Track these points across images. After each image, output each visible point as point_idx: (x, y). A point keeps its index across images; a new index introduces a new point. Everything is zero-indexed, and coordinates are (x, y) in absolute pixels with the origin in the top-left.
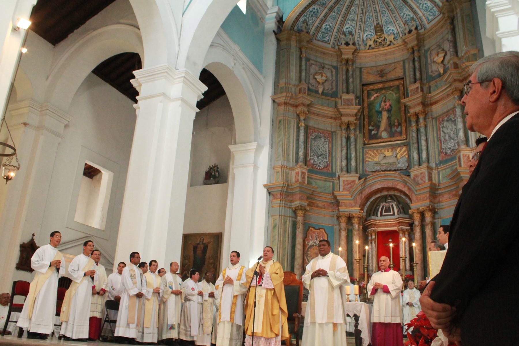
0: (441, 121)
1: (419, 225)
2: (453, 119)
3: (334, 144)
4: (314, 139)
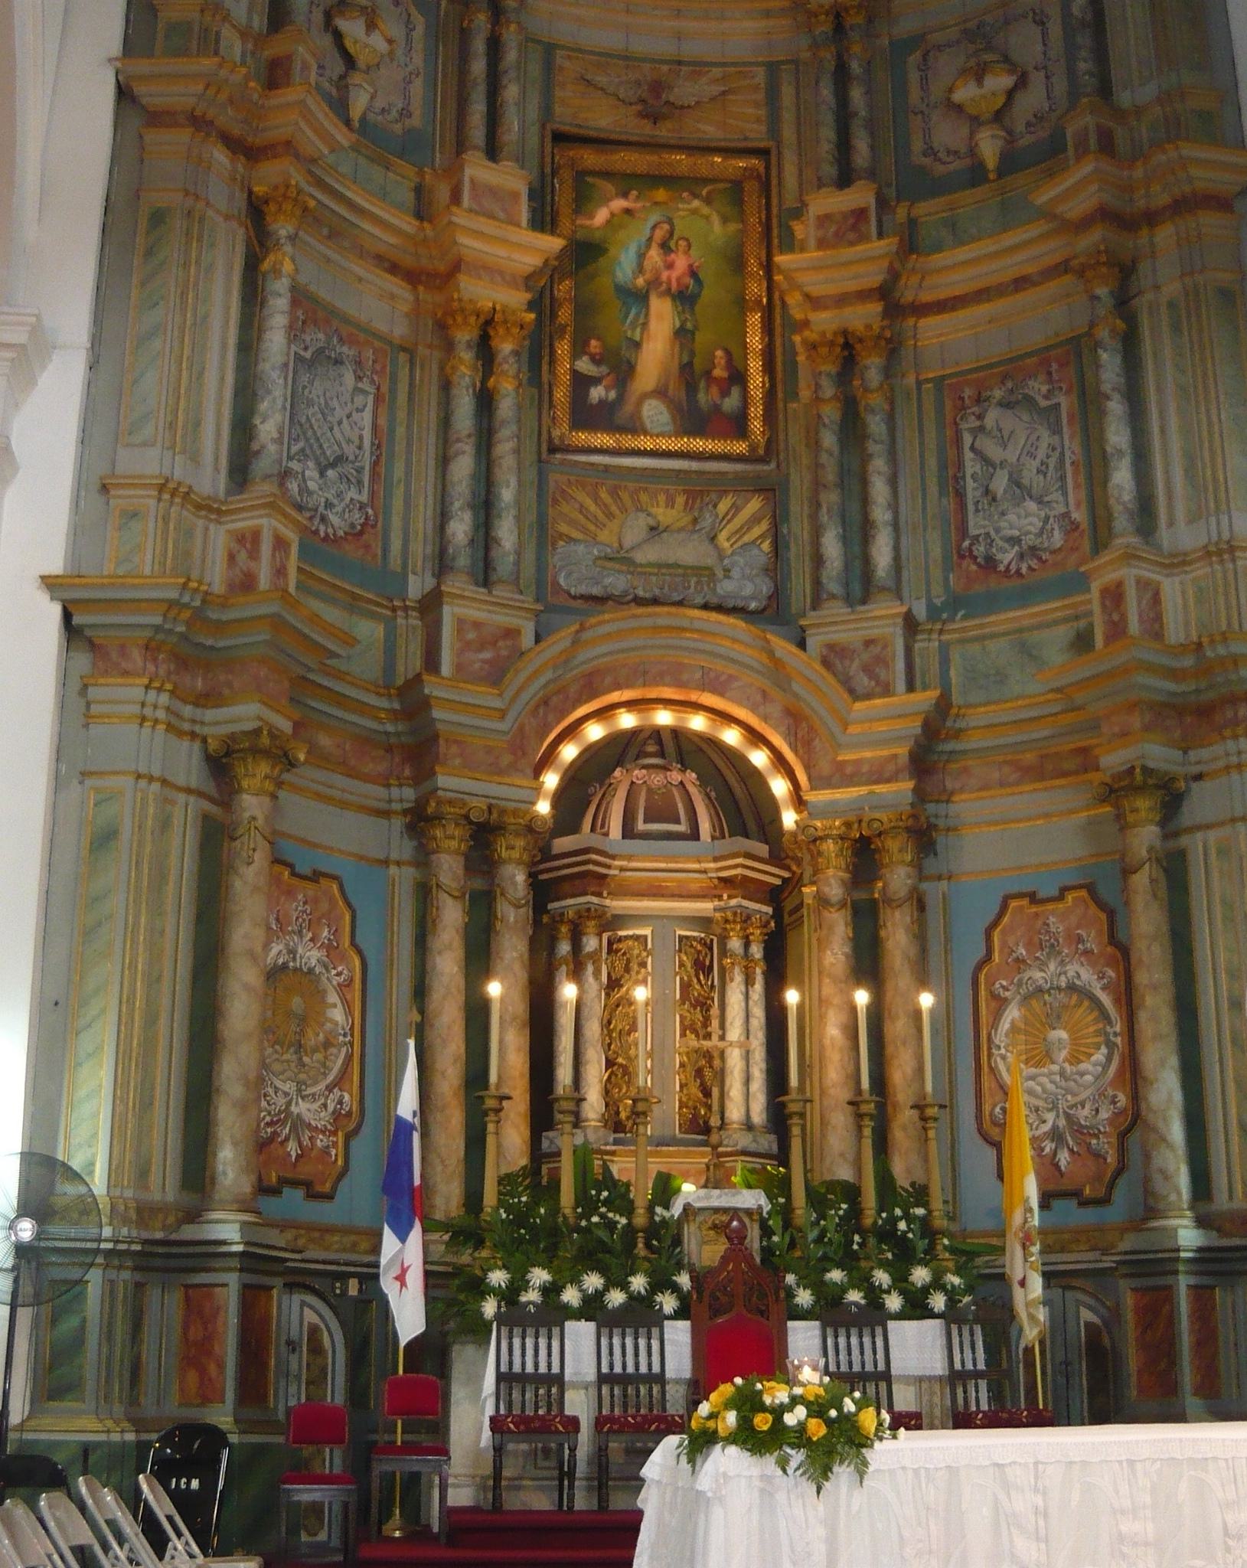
0: (967, 401)
2: (1043, 403)
3: (401, 415)
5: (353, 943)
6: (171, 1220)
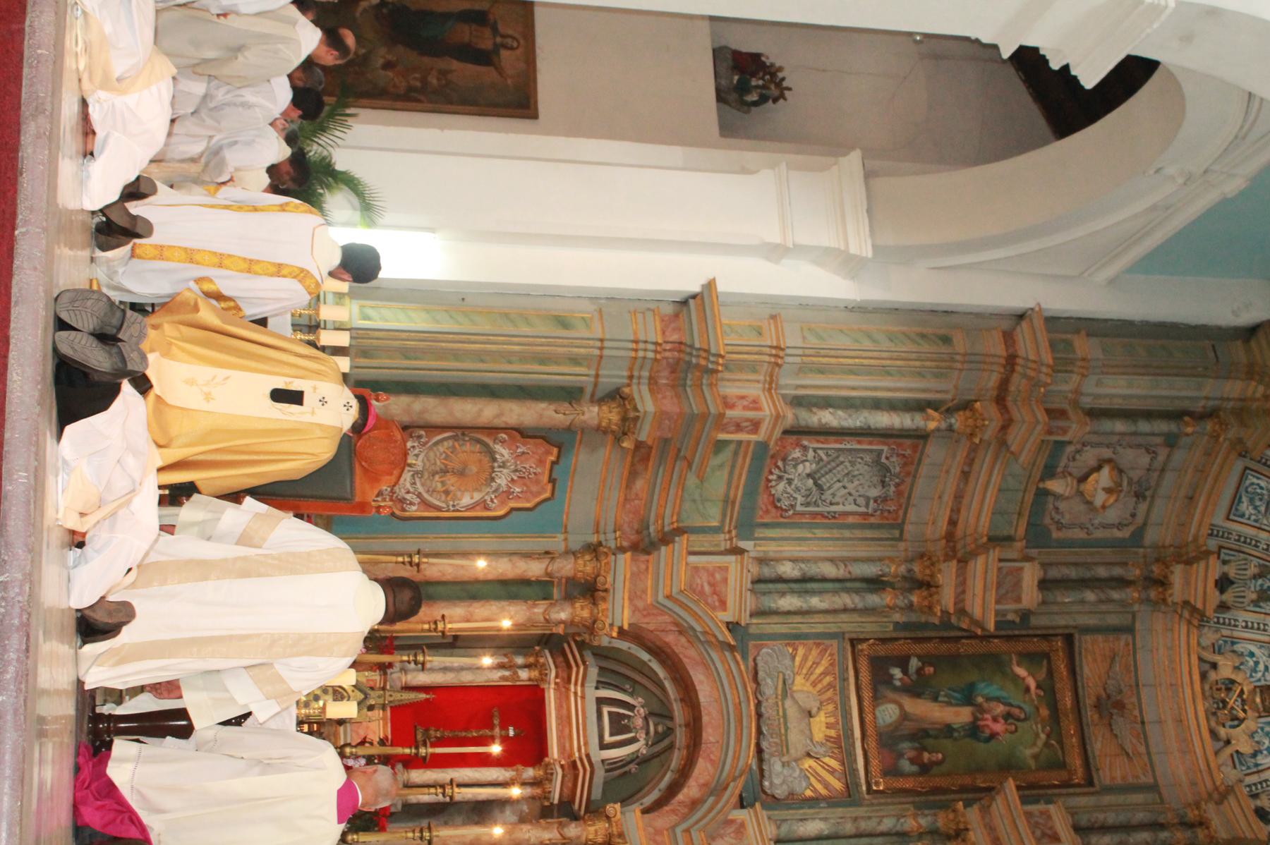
3: (858, 533)
4: (877, 462)
5: (513, 509)
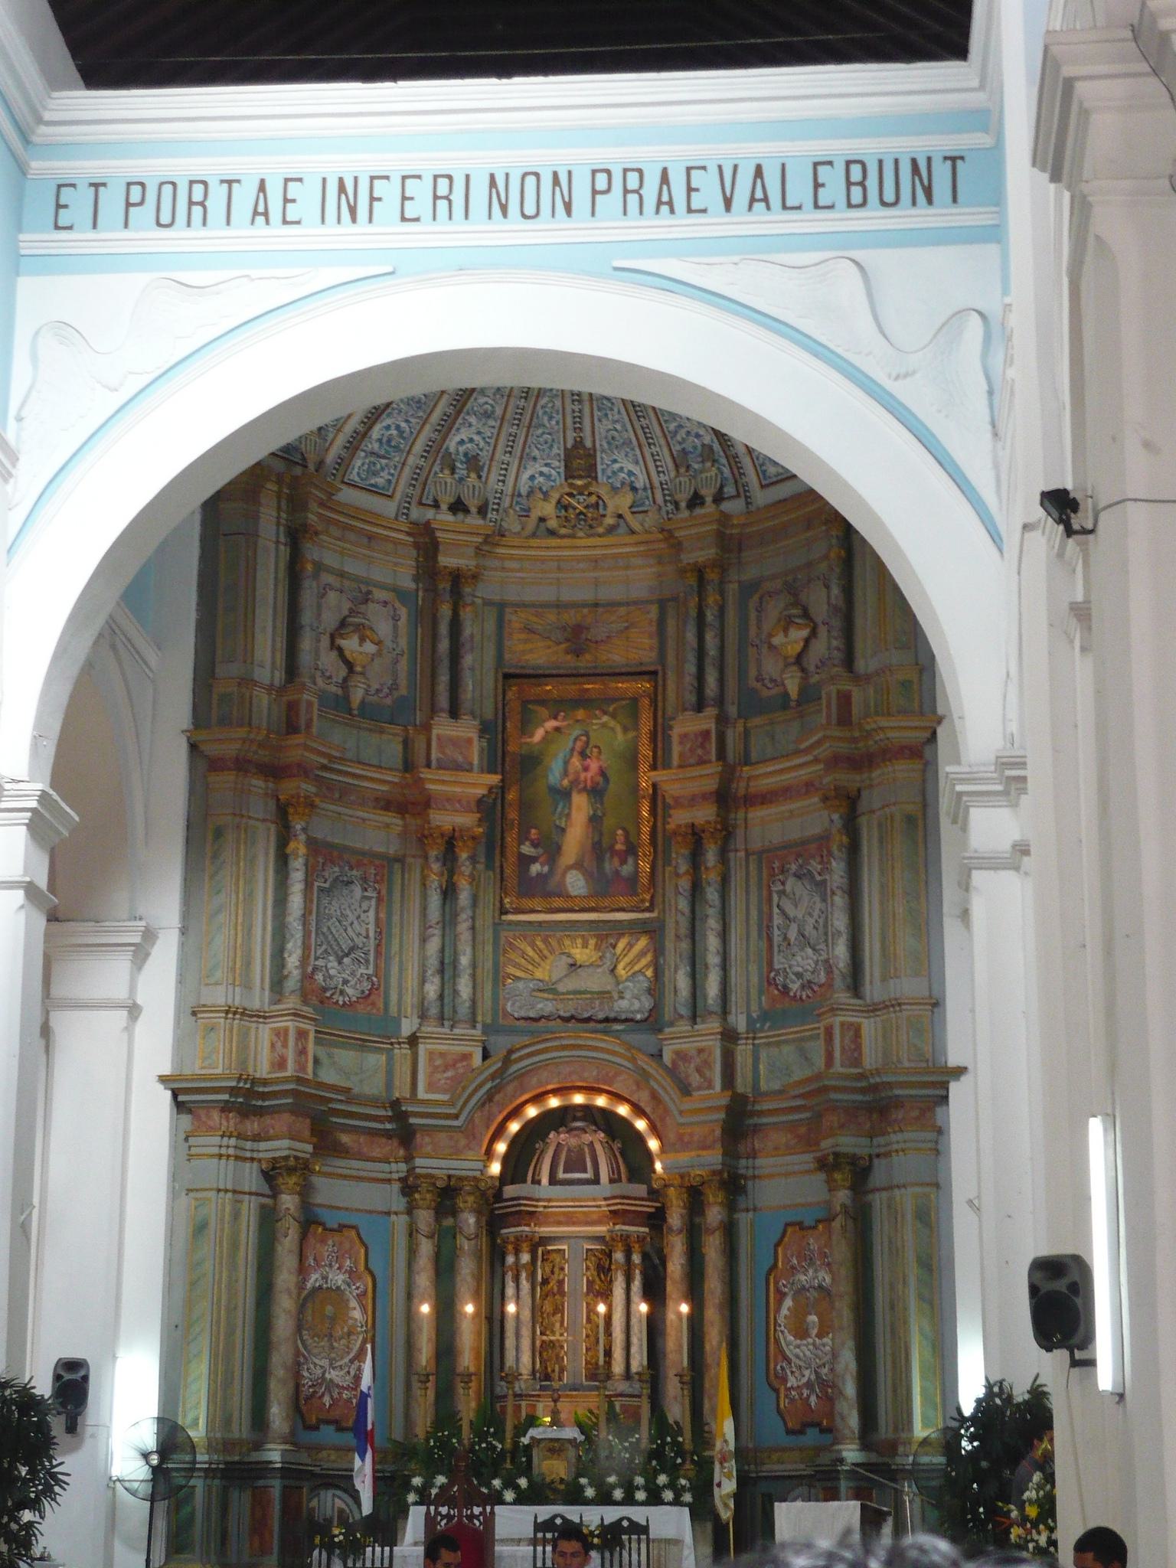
1: (680, 1231)
2: (818, 878)
3: (397, 906)
6: (244, 1449)
